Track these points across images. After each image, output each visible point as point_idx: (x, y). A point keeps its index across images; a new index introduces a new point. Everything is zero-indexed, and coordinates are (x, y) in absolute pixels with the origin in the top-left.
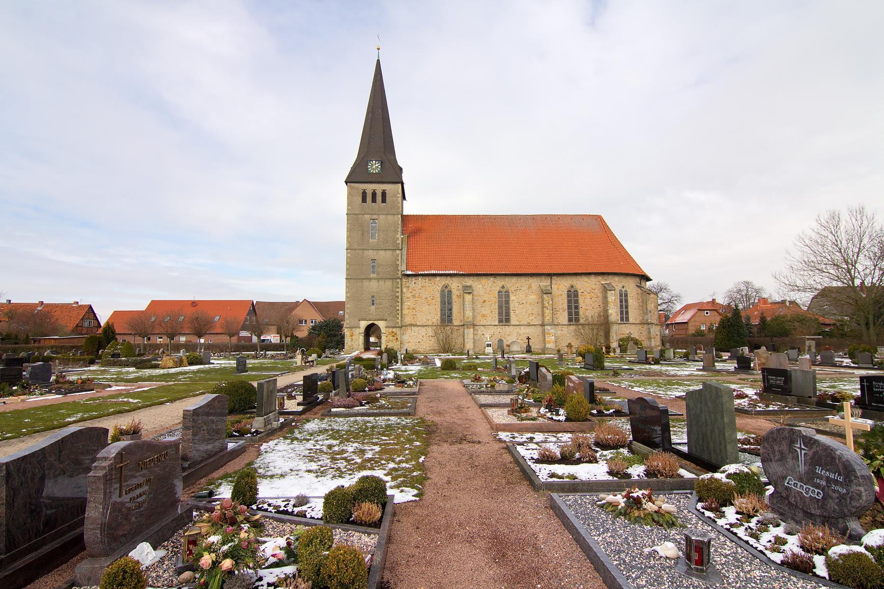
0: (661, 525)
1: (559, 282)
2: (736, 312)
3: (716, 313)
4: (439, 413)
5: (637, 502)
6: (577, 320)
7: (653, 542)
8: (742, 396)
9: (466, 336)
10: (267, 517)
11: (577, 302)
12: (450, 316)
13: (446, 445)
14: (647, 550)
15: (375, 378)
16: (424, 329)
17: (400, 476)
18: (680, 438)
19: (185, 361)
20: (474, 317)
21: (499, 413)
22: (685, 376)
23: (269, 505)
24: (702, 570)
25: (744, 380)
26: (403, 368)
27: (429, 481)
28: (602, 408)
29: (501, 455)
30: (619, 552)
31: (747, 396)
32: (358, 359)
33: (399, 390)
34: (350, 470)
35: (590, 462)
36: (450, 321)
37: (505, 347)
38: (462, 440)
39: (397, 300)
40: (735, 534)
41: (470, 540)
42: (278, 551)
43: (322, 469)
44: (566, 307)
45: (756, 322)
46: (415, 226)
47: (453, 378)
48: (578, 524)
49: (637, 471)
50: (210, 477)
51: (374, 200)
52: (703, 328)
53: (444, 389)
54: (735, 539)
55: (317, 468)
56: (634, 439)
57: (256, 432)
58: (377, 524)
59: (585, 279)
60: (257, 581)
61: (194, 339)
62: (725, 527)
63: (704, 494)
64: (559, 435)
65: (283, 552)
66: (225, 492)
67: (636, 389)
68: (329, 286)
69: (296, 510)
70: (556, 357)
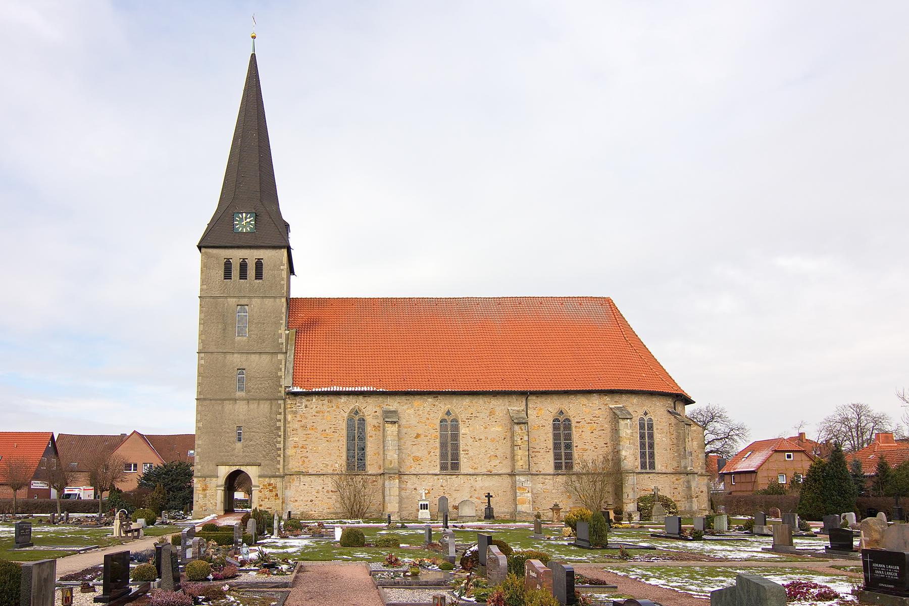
2: (836, 453)
6: (569, 466)
9: (387, 492)
11: (568, 437)
12: (362, 458)
15: (229, 559)
16: (319, 480)
20: (401, 461)
22: (742, 560)
25: (839, 568)
26: (280, 542)
31: (836, 596)
32: (210, 528)
33: (263, 578)
36: (362, 467)
37: (450, 509)
39: (276, 433)
44: (551, 446)
45: (870, 471)
46: (307, 316)
47: (356, 559)
51: (243, 275)
52: (782, 481)
53: (336, 578)
59: (583, 400)
67: (653, 582)
70: (529, 525)
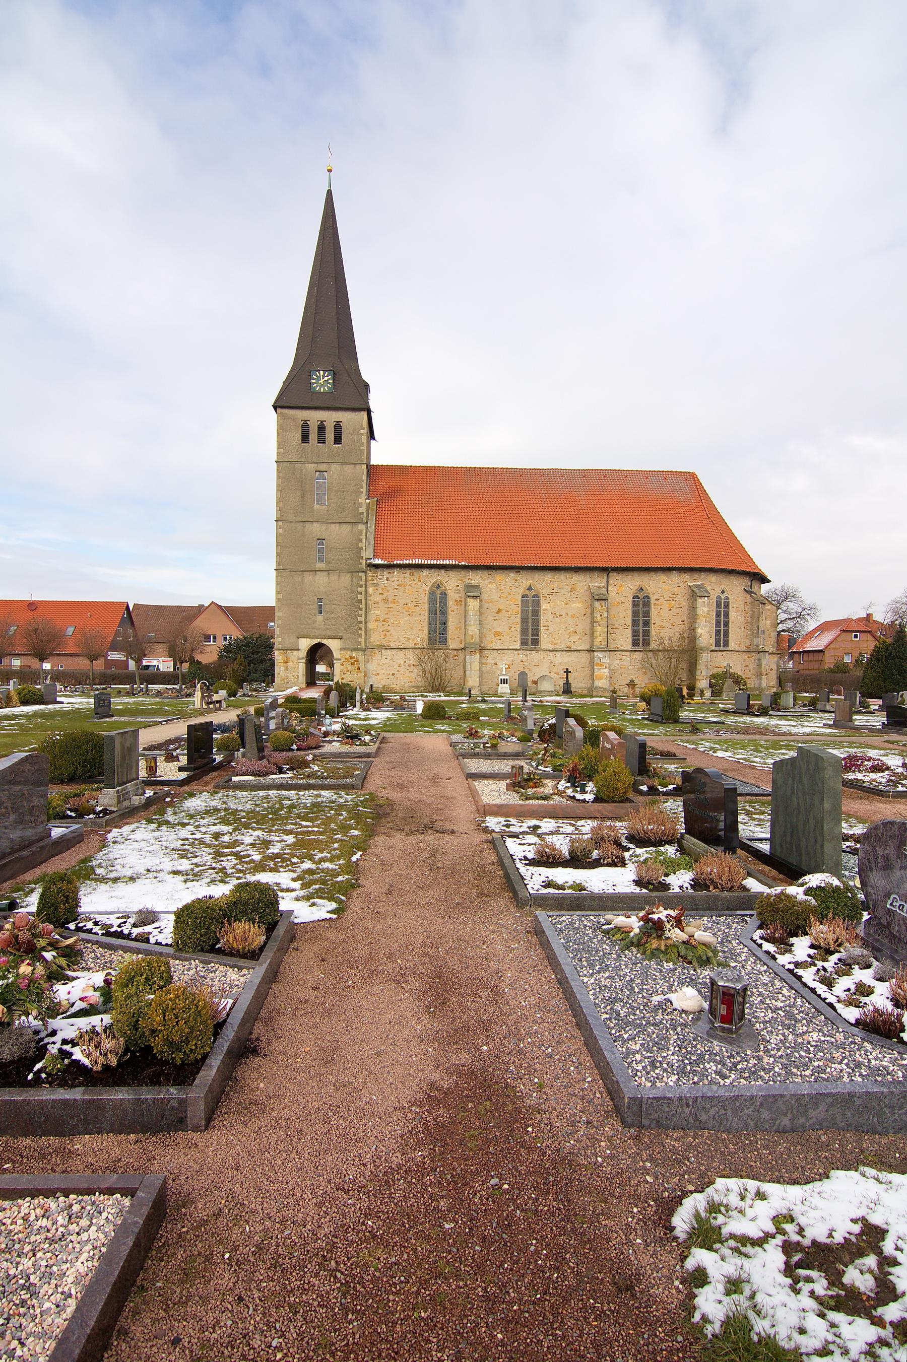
0: (690, 963)
1: (620, 582)
3: (870, 637)
4: (402, 787)
5: (658, 927)
6: (646, 643)
7: (670, 987)
8: (879, 768)
9: (468, 667)
10: (88, 941)
11: (647, 614)
12: (444, 633)
13: (399, 836)
14: (656, 999)
15: (312, 730)
16: (401, 654)
17: (314, 882)
18: (755, 829)
19: (15, 699)
20: (482, 636)
21: (494, 787)
22: (804, 734)
23: (96, 923)
24: (730, 1031)
26: (363, 714)
27: (360, 890)
28: (656, 782)
29: (481, 852)
30: (615, 1000)
31: (888, 768)
32: (292, 700)
33: (346, 748)
34: (240, 871)
35: (613, 865)
36: (444, 641)
37: (530, 684)
38: (429, 827)
39: (357, 605)
40: (799, 978)
41: (399, 979)
42: (90, 993)
43: (197, 869)
44: (629, 622)
48: (564, 957)
49: (680, 880)
50: (19, 879)
51: (321, 439)
52: (847, 660)
53: (418, 749)
54: (797, 985)
55: (189, 867)
56: (689, 831)
57: (105, 811)
58: (254, 955)
59: (662, 577)
60: (48, 1036)
61: (34, 663)
62: (788, 966)
63: (768, 917)
64: (580, 823)
65: (97, 994)
66: (31, 903)
67: (720, 754)
68: (246, 578)
69: (136, 931)
